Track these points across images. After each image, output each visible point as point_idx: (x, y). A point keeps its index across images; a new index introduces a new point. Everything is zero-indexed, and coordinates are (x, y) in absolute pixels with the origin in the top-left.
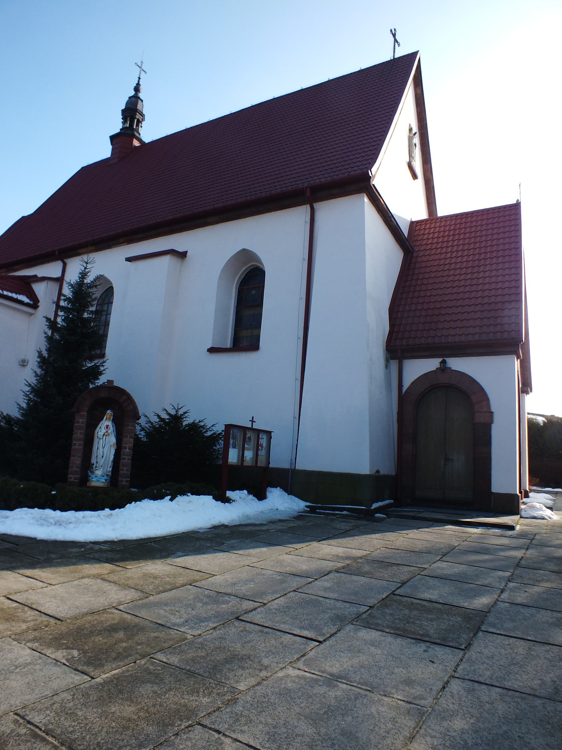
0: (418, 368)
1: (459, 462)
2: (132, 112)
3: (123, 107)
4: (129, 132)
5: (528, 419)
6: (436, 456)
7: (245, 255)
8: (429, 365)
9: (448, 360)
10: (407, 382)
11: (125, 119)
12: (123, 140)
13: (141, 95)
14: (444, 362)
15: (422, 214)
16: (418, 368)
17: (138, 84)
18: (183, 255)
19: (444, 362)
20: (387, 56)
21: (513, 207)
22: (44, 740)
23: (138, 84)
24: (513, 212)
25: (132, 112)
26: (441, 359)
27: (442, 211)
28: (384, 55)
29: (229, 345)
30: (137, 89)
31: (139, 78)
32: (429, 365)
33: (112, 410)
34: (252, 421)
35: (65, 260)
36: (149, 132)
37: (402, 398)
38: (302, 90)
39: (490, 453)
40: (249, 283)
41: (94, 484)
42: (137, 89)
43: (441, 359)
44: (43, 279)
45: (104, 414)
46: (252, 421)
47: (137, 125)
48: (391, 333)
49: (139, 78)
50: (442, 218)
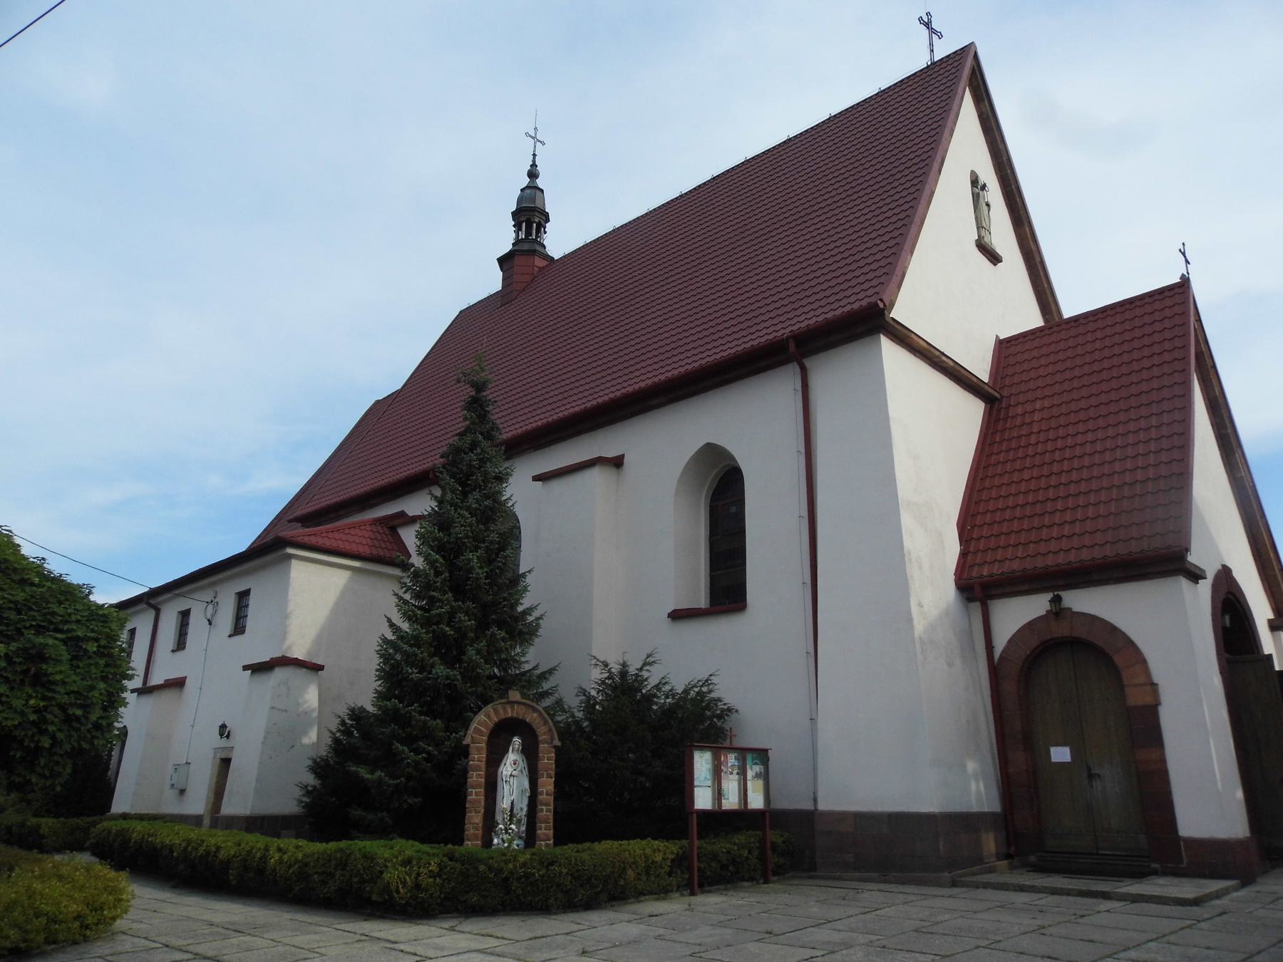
0: (1015, 615)
1: (1111, 784)
2: (530, 215)
3: (506, 247)
4: (526, 247)
5: (560, 839)
6: (1062, 777)
9: (1063, 594)
10: (1001, 639)
11: (518, 226)
12: (523, 260)
13: (540, 182)
14: (1056, 600)
15: (1032, 319)
16: (1015, 615)
17: (534, 165)
18: (617, 462)
19: (1056, 600)
20: (922, 62)
21: (1167, 294)
23: (534, 165)
24: (1178, 299)
25: (530, 215)
26: (1050, 596)
27: (1070, 307)
28: (911, 57)
29: (702, 602)
30: (533, 174)
31: (534, 155)
33: (521, 736)
36: (560, 240)
37: (995, 671)
38: (832, 119)
39: (1163, 761)
40: (722, 488)
41: (1053, 750)
42: (533, 174)
43: (1050, 596)
45: (509, 742)
47: (538, 231)
48: (963, 555)
49: (534, 155)
50: (1076, 320)
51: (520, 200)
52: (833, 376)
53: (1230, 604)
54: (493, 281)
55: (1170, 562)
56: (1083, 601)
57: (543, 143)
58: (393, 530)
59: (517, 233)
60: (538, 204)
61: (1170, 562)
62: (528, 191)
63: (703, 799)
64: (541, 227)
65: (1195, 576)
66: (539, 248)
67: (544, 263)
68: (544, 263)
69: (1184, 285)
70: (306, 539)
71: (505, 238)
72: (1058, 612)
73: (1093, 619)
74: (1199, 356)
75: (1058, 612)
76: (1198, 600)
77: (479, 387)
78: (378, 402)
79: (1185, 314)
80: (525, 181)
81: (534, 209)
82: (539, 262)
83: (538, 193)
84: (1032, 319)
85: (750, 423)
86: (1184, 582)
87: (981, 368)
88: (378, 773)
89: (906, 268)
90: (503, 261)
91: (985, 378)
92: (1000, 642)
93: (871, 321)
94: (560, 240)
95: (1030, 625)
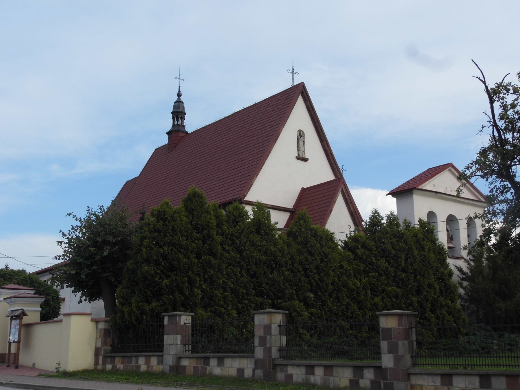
2: (178, 113)
4: (176, 128)
12: (177, 133)
13: (182, 98)
17: (179, 91)
23: (179, 91)
25: (178, 113)
30: (179, 95)
31: (179, 87)
36: (193, 123)
42: (179, 95)
49: (179, 87)
51: (174, 107)
54: (164, 140)
57: (183, 80)
59: (174, 121)
60: (181, 110)
62: (177, 104)
63: (179, 337)
64: (183, 118)
66: (181, 128)
67: (184, 134)
68: (184, 134)
71: (168, 124)
77: (68, 214)
78: (128, 182)
81: (179, 112)
82: (181, 135)
83: (181, 104)
89: (253, 182)
90: (168, 133)
91: (426, 220)
94: (193, 123)
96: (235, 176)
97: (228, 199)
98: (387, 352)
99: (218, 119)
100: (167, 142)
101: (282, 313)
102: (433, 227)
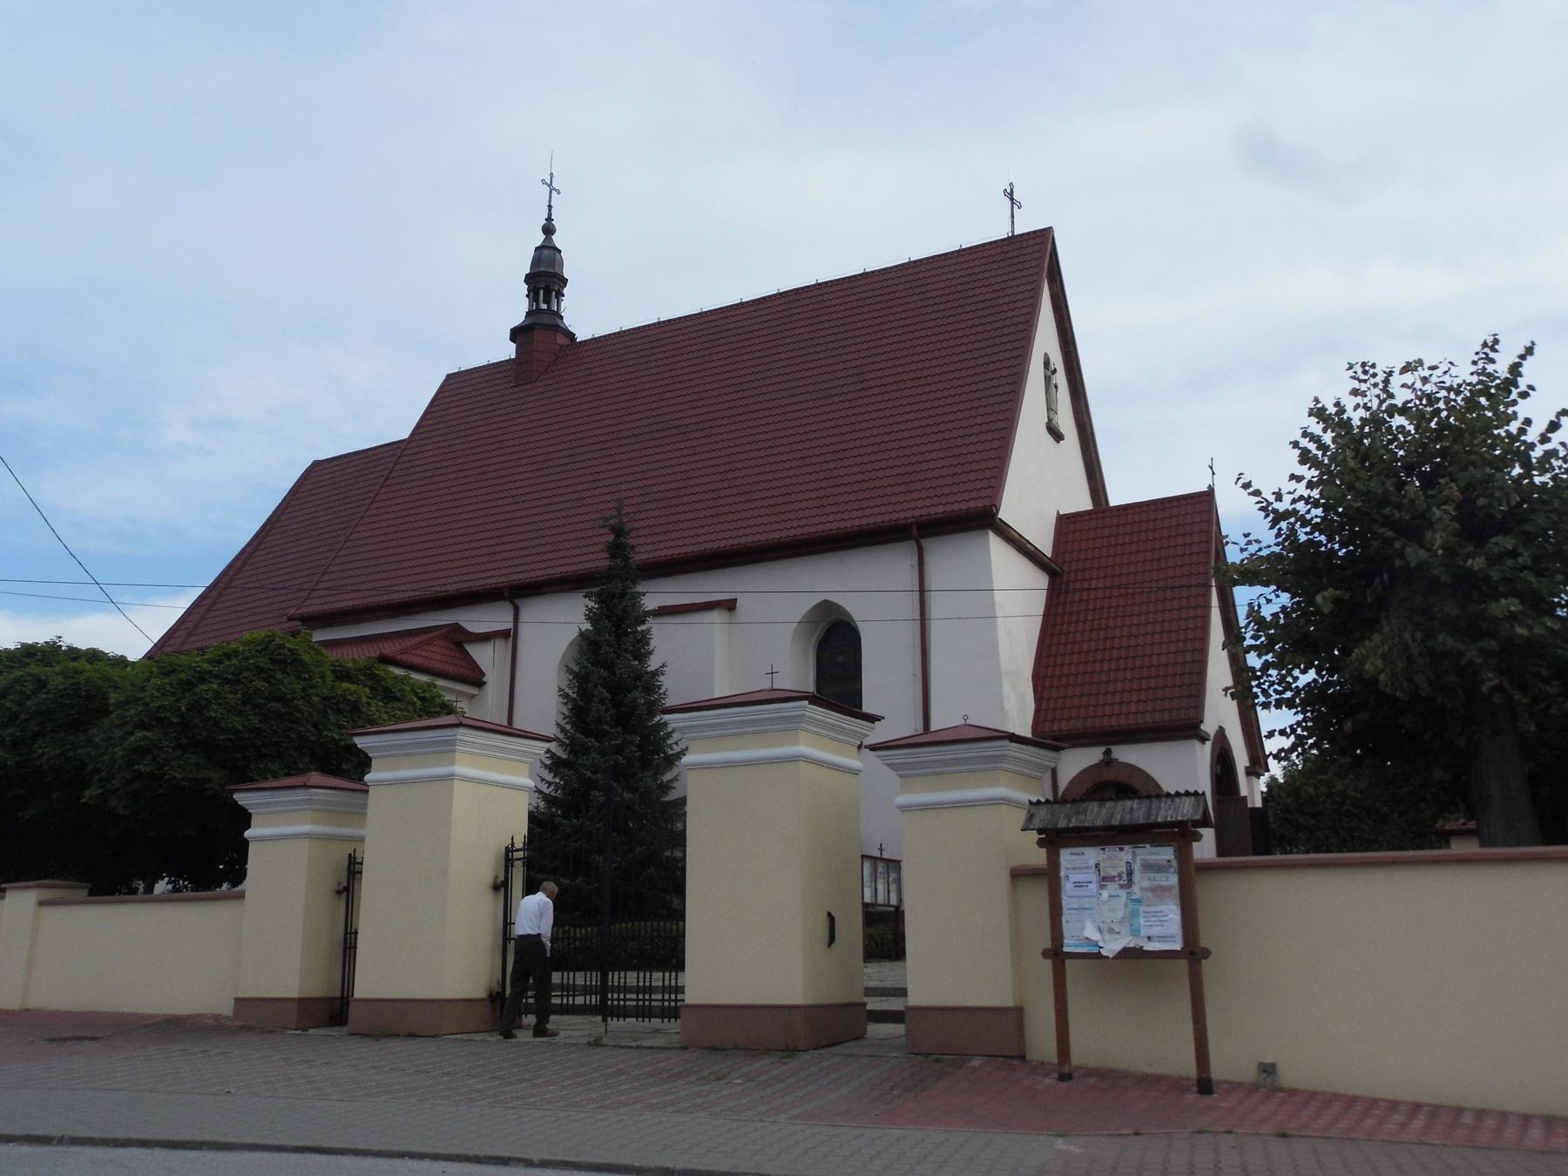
0: (1075, 762)
2: (545, 279)
3: (519, 318)
7: (827, 608)
8: (1089, 757)
9: (1113, 748)
11: (533, 294)
12: (540, 331)
13: (557, 239)
14: (1108, 753)
15: (1084, 503)
16: (1075, 762)
17: (549, 219)
18: (730, 606)
19: (1108, 753)
20: (1000, 232)
22: (1055, 739)
23: (549, 219)
25: (545, 279)
26: (1103, 749)
27: (1116, 498)
30: (548, 230)
31: (550, 207)
32: (1089, 757)
33: (1254, 810)
34: (881, 850)
35: (517, 601)
36: (588, 314)
42: (548, 230)
43: (1103, 749)
44: (485, 638)
46: (881, 850)
48: (1037, 712)
49: (550, 207)
51: (536, 262)
52: (948, 560)
53: (1223, 758)
55: (1188, 728)
56: (1127, 754)
58: (459, 646)
61: (1188, 728)
62: (546, 252)
65: (1203, 739)
69: (1209, 495)
70: (404, 657)
71: (516, 308)
72: (1108, 761)
73: (1134, 768)
74: (1217, 552)
75: (1108, 761)
76: (1203, 754)
78: (316, 464)
79: (1209, 521)
80: (540, 238)
84: (1084, 503)
85: (870, 588)
86: (1197, 743)
87: (1045, 544)
88: (578, 880)
92: (1063, 782)
93: (984, 519)
95: (1086, 771)
96: (529, 520)
97: (588, 566)
98: (903, 999)
99: (950, 246)
100: (581, 336)
101: (1159, 794)
102: (134, 891)
